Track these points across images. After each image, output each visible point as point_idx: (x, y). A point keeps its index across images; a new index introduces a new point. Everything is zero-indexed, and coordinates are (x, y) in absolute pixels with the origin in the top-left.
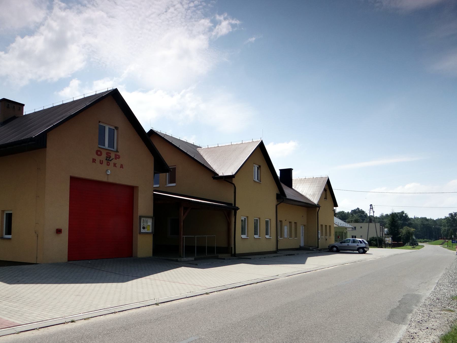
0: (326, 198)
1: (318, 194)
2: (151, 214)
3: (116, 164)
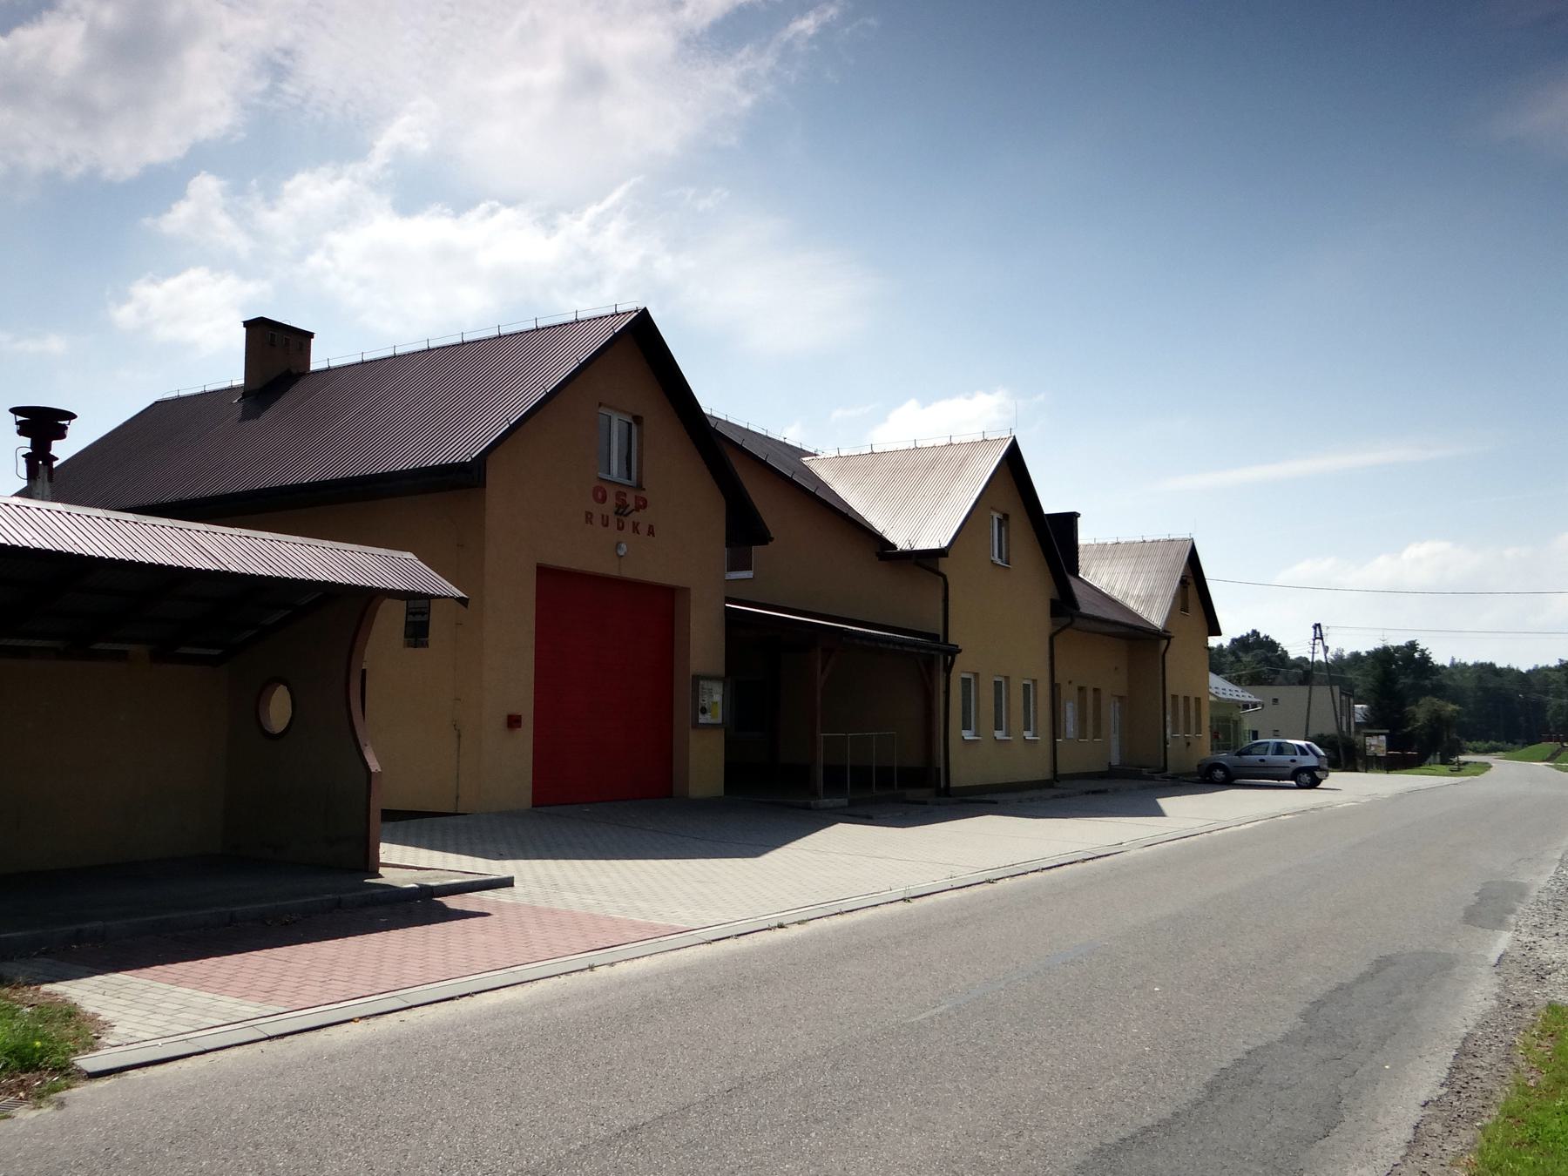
0: (1185, 608)
1: (1164, 595)
2: (721, 671)
3: (638, 524)
